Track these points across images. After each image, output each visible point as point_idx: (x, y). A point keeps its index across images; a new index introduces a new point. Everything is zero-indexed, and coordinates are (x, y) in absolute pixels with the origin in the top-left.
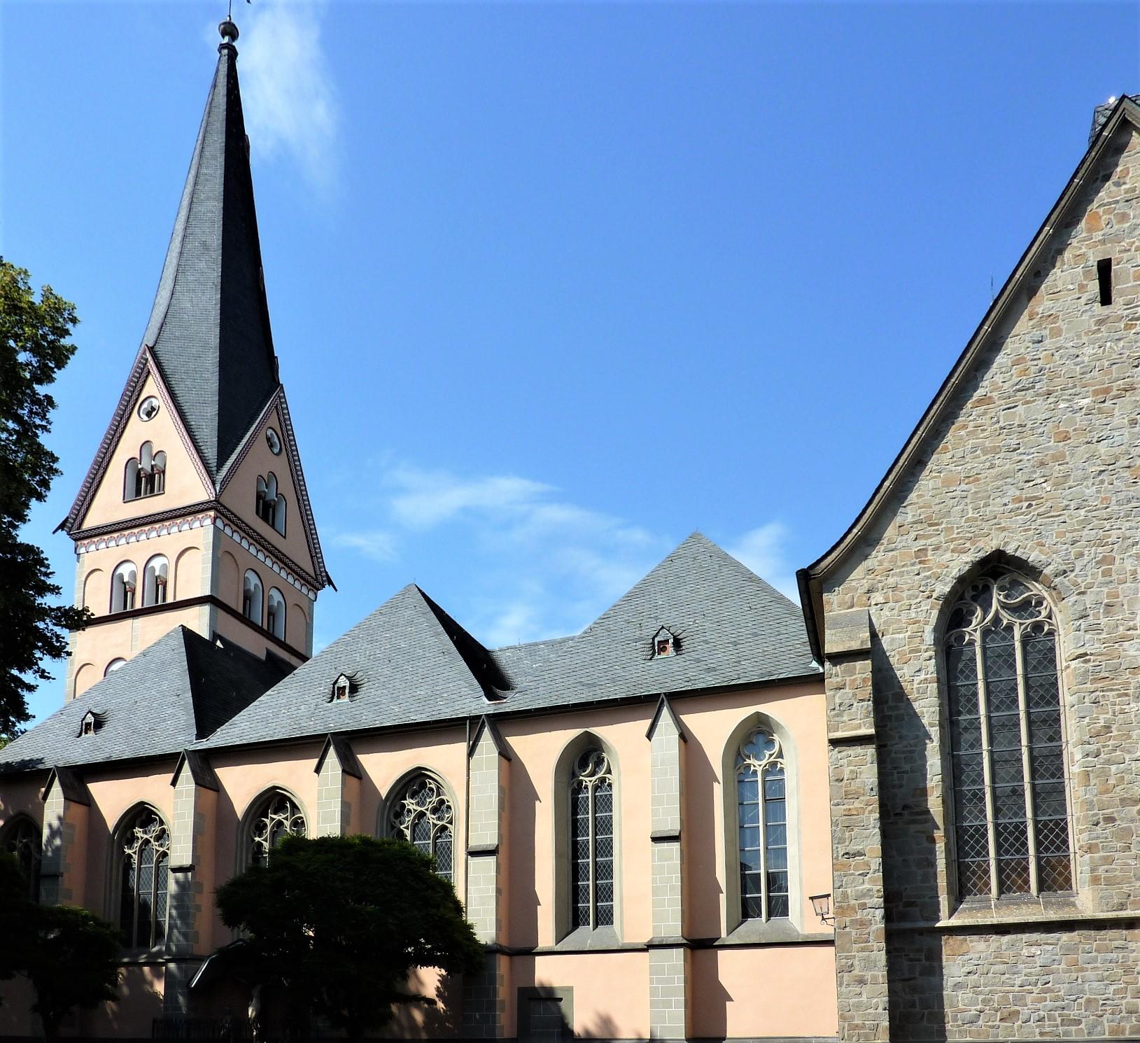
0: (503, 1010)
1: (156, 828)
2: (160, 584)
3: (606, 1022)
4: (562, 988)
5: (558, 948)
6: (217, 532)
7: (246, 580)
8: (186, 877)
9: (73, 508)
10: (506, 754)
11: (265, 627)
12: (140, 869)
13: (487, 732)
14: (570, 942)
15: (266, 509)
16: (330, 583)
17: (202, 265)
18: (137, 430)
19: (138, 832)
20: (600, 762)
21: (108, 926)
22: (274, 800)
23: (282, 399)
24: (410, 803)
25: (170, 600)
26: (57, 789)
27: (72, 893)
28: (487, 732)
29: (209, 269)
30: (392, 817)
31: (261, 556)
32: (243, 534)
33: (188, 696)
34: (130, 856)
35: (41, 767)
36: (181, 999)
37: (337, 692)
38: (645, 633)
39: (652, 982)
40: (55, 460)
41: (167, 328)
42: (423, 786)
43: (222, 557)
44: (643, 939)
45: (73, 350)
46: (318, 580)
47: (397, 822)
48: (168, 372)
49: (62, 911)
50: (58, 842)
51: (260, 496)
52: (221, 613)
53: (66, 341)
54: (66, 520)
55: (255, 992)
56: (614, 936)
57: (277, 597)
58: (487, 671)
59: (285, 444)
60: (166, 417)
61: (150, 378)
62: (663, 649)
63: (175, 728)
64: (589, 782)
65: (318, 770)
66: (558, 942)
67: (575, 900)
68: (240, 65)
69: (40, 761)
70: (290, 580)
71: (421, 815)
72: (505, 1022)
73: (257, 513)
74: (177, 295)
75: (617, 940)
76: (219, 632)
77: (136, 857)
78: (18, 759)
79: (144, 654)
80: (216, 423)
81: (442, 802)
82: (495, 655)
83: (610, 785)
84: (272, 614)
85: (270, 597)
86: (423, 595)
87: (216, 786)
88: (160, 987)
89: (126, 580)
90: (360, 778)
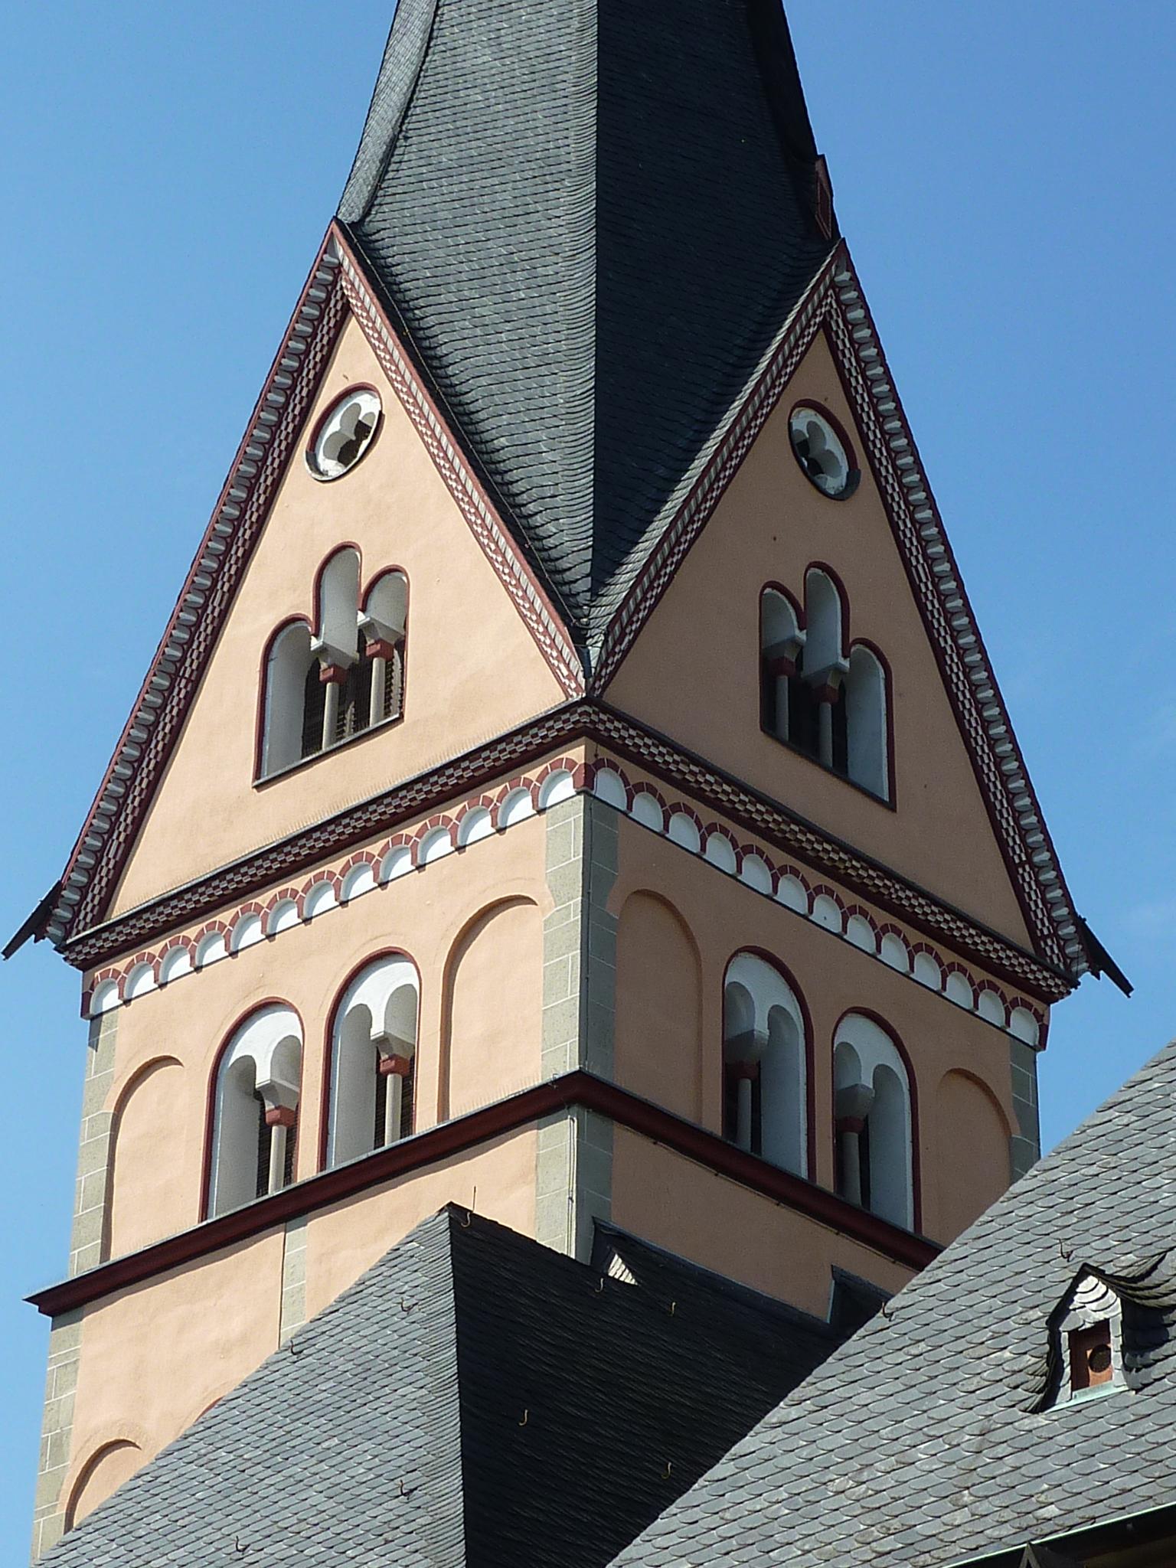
2: (393, 1064)
6: (601, 827)
7: (732, 999)
9: (81, 847)
11: (826, 1179)
15: (807, 707)
16: (1100, 961)
18: (309, 512)
23: (848, 294)
31: (791, 893)
33: (448, 1493)
41: (408, 155)
43: (623, 915)
48: (412, 289)
51: (774, 665)
52: (628, 1143)
57: (871, 1050)
59: (874, 451)
61: (352, 324)
73: (769, 724)
74: (447, 35)
76: (619, 1221)
79: (295, 1350)
84: (854, 1125)
85: (843, 1055)
89: (263, 1076)
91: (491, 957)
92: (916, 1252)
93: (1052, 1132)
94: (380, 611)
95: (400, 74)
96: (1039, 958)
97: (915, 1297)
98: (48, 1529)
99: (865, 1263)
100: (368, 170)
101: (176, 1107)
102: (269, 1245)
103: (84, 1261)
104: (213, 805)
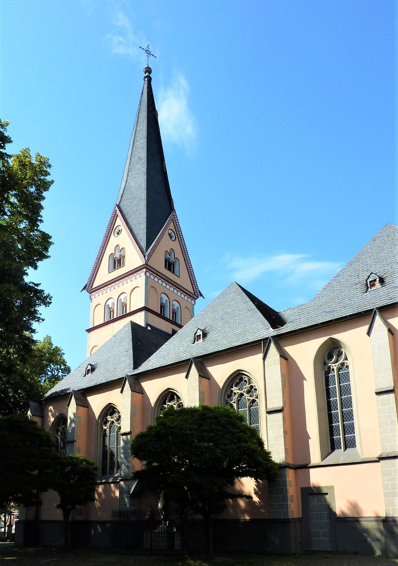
0: (292, 501)
1: (116, 415)
2: (124, 306)
3: (354, 507)
4: (326, 487)
5: (323, 463)
7: (161, 298)
8: (127, 438)
10: (284, 356)
11: (171, 319)
12: (110, 436)
13: (272, 346)
14: (330, 460)
15: (170, 265)
16: (201, 295)
17: (139, 166)
18: (114, 241)
19: (109, 418)
20: (340, 354)
21: (93, 464)
22: (169, 395)
24: (235, 389)
25: (128, 312)
26: (73, 401)
27: (80, 451)
28: (272, 346)
29: (141, 167)
30: (227, 398)
32: (171, 285)
34: (106, 430)
35: (68, 392)
36: (126, 500)
37: (197, 338)
38: (361, 279)
39: (383, 481)
40: (50, 237)
41: (124, 196)
42: (241, 379)
43: (149, 288)
44: (375, 455)
45: (52, 182)
46: (195, 294)
47: (229, 400)
48: (125, 213)
49: (71, 458)
50: (73, 425)
51: (166, 261)
52: (150, 314)
53: (49, 178)
54: (86, 285)
55: (161, 495)
56: (357, 454)
58: (274, 318)
59: (178, 235)
60: (125, 232)
62: (373, 285)
63: (125, 368)
64: (335, 366)
65: (187, 377)
66: (322, 460)
67: (332, 434)
68: (152, 83)
69: (68, 389)
70: (182, 296)
71: (242, 395)
72: (294, 509)
73: (166, 267)
75: (359, 457)
76: (149, 323)
77: (108, 430)
78: (60, 390)
80: (145, 231)
81: (252, 387)
82: (281, 314)
83: (347, 367)
84: (174, 313)
85: (173, 305)
86: (240, 286)
87: (142, 392)
88: (117, 494)
90: (209, 379)
91: (135, 293)
92: (181, 327)
93: (196, 314)
94: (122, 253)
95: (123, 186)
96: (195, 295)
97: (180, 331)
98: (88, 355)
99: (175, 328)
100: (120, 198)
101: (101, 309)
102: (111, 325)
103: (91, 326)
104: (103, 276)
